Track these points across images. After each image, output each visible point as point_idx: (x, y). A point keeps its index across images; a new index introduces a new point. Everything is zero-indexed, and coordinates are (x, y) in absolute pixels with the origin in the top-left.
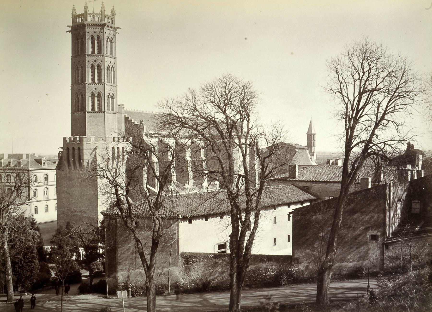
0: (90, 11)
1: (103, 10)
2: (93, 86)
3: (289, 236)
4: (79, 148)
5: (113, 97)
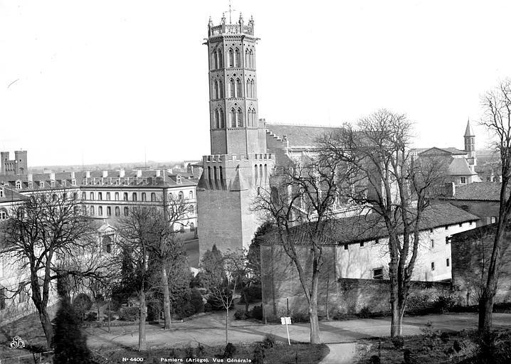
0: (227, 23)
1: (241, 21)
2: (233, 102)
3: (448, 260)
4: (221, 167)
5: (254, 111)
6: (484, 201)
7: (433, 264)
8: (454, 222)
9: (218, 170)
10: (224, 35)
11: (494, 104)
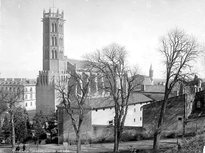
0: (52, 12)
1: (58, 12)
2: (53, 47)
3: (141, 118)
4: (46, 76)
5: (62, 52)
6: (157, 93)
7: (135, 119)
8: (144, 101)
9: (45, 77)
10: (50, 17)
11: (165, 42)
